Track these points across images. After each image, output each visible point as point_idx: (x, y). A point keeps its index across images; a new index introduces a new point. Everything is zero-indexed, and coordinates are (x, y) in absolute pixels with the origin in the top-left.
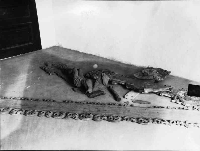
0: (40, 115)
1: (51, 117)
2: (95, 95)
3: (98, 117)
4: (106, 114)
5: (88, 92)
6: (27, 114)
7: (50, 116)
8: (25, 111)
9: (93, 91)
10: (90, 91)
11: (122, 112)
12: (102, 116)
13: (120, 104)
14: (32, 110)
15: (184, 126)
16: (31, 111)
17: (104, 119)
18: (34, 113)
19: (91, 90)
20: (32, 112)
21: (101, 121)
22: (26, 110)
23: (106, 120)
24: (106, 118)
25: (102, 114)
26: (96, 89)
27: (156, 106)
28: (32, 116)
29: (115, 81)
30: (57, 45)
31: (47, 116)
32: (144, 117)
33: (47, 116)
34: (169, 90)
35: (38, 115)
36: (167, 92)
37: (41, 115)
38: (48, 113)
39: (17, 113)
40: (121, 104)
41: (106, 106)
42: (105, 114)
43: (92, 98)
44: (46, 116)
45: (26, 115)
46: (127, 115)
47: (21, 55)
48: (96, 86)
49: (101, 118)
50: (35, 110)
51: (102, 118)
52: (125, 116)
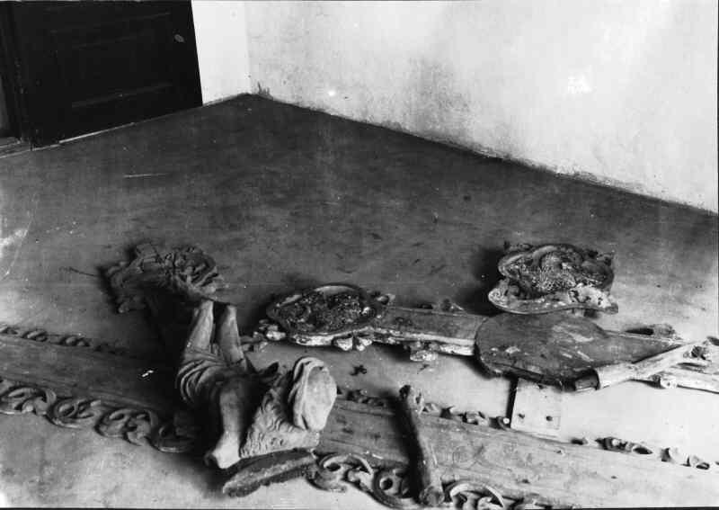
0: (103, 429)
1: (144, 444)
2: (259, 477)
3: (334, 467)
4: (374, 456)
5: (214, 463)
6: (56, 418)
7: (140, 435)
8: (58, 397)
9: (245, 456)
10: (227, 454)
11: (448, 453)
12: (356, 466)
13: (448, 410)
14: (83, 400)
15: (679, 386)
16: (78, 402)
17: (357, 484)
18: (84, 414)
19: (236, 447)
20: (82, 408)
21: (343, 489)
22: (61, 394)
23: (368, 492)
24: (366, 479)
25: (356, 456)
26: (260, 446)
27: (611, 440)
28: (72, 426)
29: (419, 345)
30: (248, 88)
31: (130, 435)
32: (543, 499)
33: (130, 435)
34: (694, 356)
35: (97, 428)
36: (686, 366)
37: (108, 426)
38: (137, 422)
39: (19, 408)
40: (452, 411)
41: (433, 312)
42: (369, 457)
43: (238, 495)
44: (125, 438)
45: (53, 420)
46: (469, 474)
47: (132, 123)
48: (257, 431)
49: (345, 478)
50: (94, 400)
51: (350, 474)
52: (457, 478)
